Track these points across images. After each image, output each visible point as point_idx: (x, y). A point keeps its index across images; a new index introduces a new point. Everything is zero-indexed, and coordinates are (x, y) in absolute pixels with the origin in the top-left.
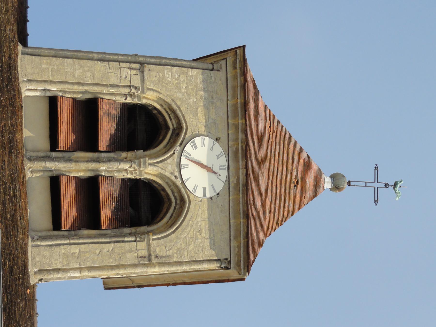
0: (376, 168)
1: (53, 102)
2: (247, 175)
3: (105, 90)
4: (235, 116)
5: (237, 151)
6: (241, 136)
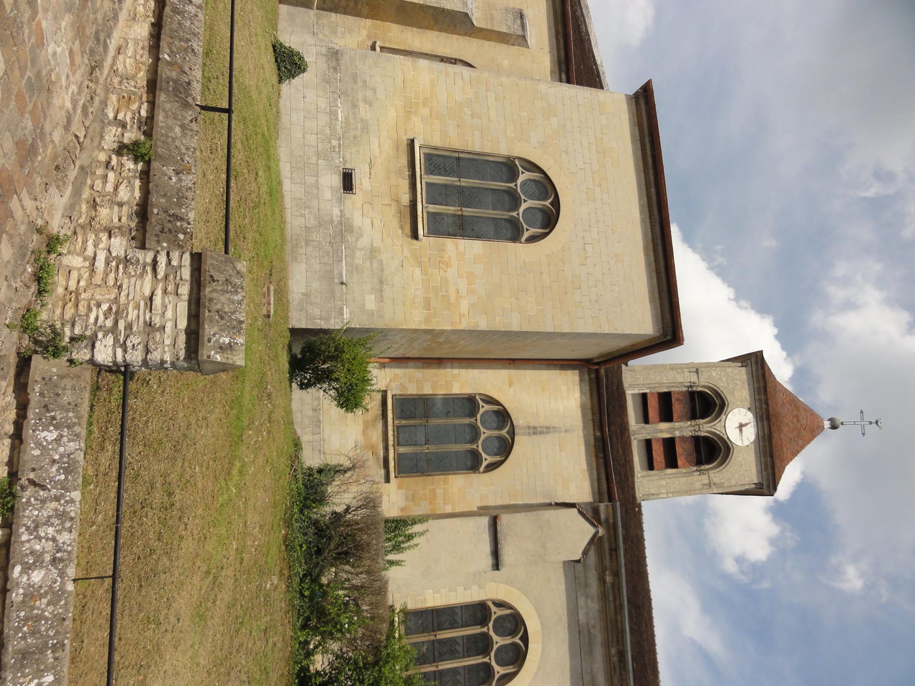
0: (863, 434)
2: (770, 430)
4: (759, 393)
6: (764, 406)
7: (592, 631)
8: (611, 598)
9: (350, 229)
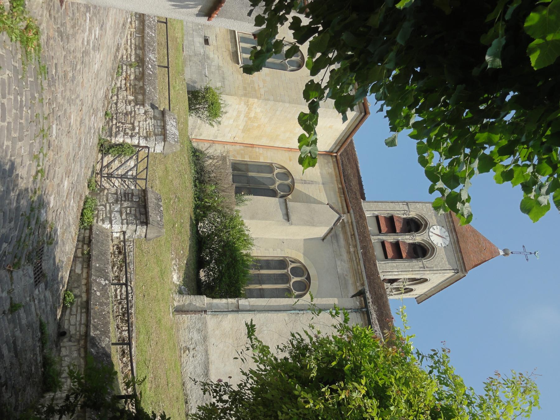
1: (377, 218)
3: (396, 212)
4: (448, 218)
5: (451, 230)
7: (346, 277)
8: (354, 259)
9: (208, 58)
